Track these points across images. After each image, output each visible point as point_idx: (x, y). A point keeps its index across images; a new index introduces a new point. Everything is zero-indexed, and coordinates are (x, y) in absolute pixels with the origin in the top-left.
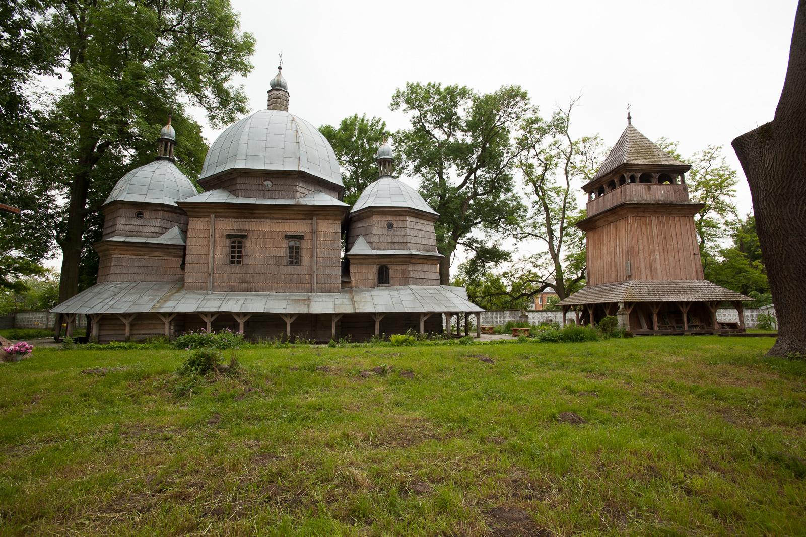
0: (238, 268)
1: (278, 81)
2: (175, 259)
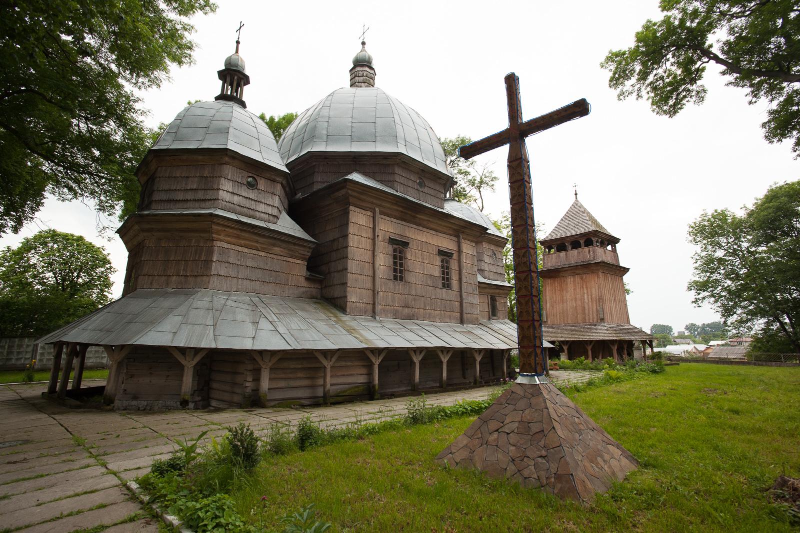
0: (400, 287)
2: (298, 261)
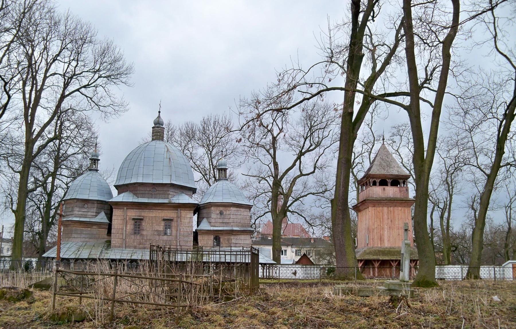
1: (158, 121)
